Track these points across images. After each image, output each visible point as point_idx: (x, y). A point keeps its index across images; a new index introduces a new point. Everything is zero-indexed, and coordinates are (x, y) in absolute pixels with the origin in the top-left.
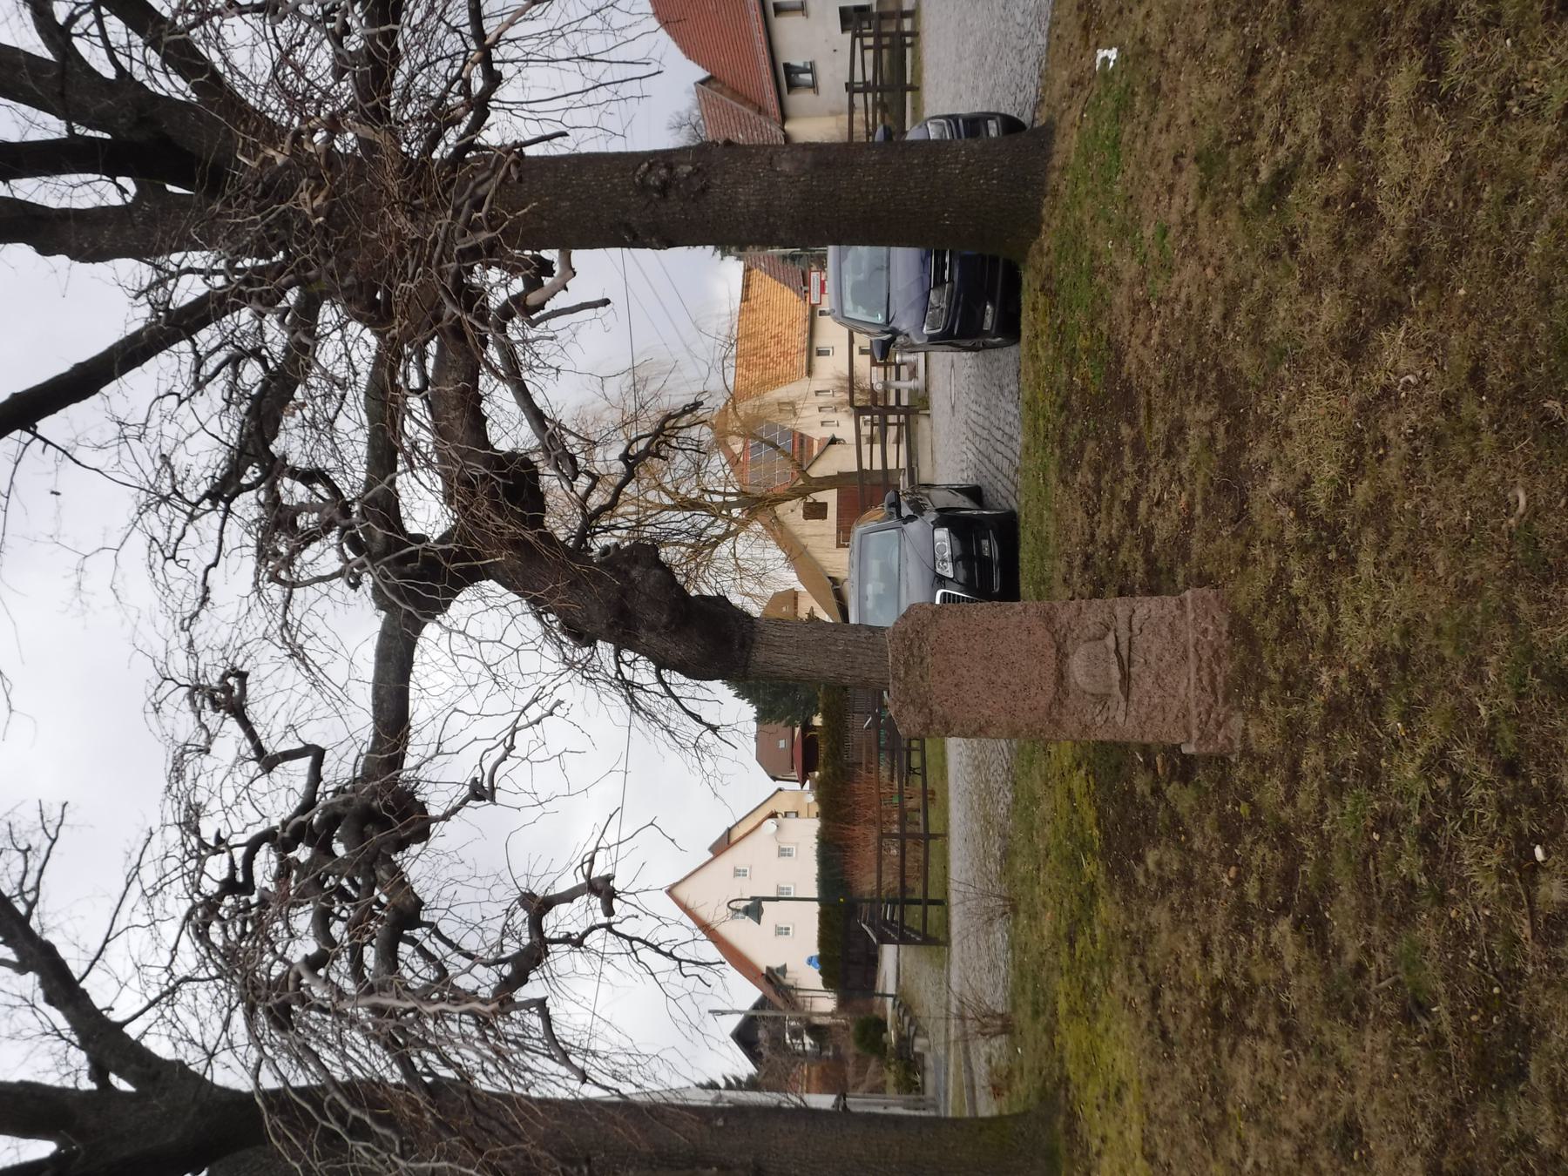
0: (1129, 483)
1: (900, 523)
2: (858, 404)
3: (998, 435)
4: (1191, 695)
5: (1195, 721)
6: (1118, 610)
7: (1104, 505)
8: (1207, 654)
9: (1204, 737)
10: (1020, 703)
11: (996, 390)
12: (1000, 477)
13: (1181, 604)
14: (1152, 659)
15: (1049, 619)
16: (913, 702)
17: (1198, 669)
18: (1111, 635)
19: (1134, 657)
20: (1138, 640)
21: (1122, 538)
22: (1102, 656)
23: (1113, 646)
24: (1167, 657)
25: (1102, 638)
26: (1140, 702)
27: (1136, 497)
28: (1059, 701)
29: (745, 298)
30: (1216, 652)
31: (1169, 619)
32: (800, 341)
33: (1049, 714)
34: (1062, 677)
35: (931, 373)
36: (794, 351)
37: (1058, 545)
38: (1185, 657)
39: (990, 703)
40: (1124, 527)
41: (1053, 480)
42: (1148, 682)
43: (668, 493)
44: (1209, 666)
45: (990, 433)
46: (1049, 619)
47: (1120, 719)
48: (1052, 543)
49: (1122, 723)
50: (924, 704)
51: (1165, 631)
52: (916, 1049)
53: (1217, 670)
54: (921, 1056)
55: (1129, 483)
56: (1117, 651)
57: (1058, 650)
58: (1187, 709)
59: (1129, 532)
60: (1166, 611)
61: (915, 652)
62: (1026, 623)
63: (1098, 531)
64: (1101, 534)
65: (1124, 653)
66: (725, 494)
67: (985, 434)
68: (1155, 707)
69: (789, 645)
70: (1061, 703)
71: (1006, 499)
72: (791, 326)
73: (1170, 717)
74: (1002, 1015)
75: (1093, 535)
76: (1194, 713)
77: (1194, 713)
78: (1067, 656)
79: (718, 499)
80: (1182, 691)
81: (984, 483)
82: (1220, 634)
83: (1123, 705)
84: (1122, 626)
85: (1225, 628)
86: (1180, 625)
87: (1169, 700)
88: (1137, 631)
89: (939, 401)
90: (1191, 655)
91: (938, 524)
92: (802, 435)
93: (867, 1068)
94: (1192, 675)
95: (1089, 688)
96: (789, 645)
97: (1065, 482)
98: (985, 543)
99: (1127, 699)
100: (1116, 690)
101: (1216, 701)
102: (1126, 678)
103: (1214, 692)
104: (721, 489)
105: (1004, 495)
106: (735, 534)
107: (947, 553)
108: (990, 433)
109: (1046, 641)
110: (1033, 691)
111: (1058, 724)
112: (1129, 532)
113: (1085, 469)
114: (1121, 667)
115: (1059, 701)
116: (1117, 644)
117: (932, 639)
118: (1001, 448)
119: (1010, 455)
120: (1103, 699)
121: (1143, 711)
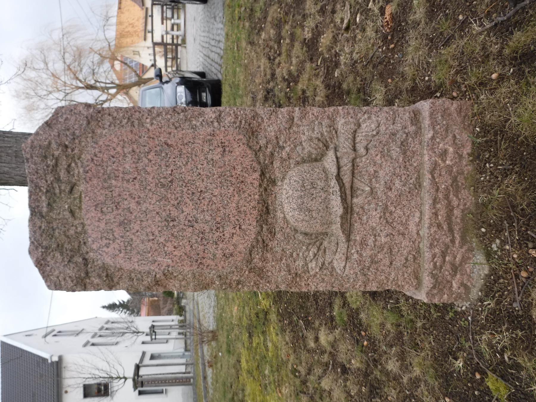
0: (310, 23)
1: (161, 85)
2: (155, 41)
3: (213, 43)
4: (424, 232)
5: (427, 266)
6: (340, 122)
7: (284, 49)
8: (445, 182)
9: (439, 284)
10: (212, 248)
11: (212, 20)
12: (213, 64)
13: (416, 118)
14: (380, 188)
15: (252, 132)
16: (60, 247)
17: (435, 201)
18: (331, 154)
19: (358, 184)
20: (362, 162)
21: (300, 71)
22: (321, 184)
23: (333, 170)
24: (398, 184)
25: (318, 159)
26: (363, 243)
27: (317, 33)
28: (262, 244)
29: (120, 8)
30: (455, 180)
31: (401, 136)
32: (141, 27)
33: (249, 261)
34: (268, 212)
35: (187, 23)
36: (139, 30)
37: (246, 87)
38: (419, 185)
39: (170, 248)
40: (303, 62)
41: (244, 44)
42: (374, 217)
43: (81, 81)
44: (447, 197)
45: (209, 44)
46: (252, 132)
47: (338, 265)
48: (242, 86)
49: (338, 268)
50: (76, 251)
51: (395, 151)
52: (182, 304)
53: (455, 202)
54: (185, 306)
55: (310, 23)
56: (339, 178)
57: (263, 174)
58: (418, 251)
59: (308, 65)
60: (398, 126)
61: (63, 174)
62: (221, 137)
63: (278, 71)
64: (281, 72)
65: (346, 179)
66: (106, 83)
67: (207, 45)
68: (382, 248)
69: (8, 155)
70: (265, 246)
71: (216, 75)
72: (138, 20)
73: (399, 262)
74: (212, 332)
75: (273, 75)
76: (427, 255)
77: (427, 255)
78: (273, 182)
79: (103, 85)
80: (412, 227)
81: (206, 70)
82: (461, 157)
83: (343, 246)
84: (345, 145)
85: (468, 149)
86: (413, 145)
87: (398, 239)
88: (362, 151)
89: (189, 39)
90: (426, 183)
91: (179, 84)
92: (143, 65)
93: (167, 301)
94: (427, 208)
95: (302, 227)
96: (8, 155)
97: (252, 43)
98: (204, 94)
99: (348, 240)
100: (336, 228)
101: (453, 241)
102: (348, 210)
103: (451, 230)
104: (104, 81)
105: (214, 74)
106: (110, 100)
107: (184, 100)
108: (209, 44)
109: (247, 162)
110: (229, 230)
111: (261, 273)
112: (308, 65)
113: (268, 26)
114: (344, 200)
115: (262, 244)
116: (339, 168)
117: (86, 157)
118: (214, 49)
119: (218, 51)
120: (317, 239)
121: (367, 253)
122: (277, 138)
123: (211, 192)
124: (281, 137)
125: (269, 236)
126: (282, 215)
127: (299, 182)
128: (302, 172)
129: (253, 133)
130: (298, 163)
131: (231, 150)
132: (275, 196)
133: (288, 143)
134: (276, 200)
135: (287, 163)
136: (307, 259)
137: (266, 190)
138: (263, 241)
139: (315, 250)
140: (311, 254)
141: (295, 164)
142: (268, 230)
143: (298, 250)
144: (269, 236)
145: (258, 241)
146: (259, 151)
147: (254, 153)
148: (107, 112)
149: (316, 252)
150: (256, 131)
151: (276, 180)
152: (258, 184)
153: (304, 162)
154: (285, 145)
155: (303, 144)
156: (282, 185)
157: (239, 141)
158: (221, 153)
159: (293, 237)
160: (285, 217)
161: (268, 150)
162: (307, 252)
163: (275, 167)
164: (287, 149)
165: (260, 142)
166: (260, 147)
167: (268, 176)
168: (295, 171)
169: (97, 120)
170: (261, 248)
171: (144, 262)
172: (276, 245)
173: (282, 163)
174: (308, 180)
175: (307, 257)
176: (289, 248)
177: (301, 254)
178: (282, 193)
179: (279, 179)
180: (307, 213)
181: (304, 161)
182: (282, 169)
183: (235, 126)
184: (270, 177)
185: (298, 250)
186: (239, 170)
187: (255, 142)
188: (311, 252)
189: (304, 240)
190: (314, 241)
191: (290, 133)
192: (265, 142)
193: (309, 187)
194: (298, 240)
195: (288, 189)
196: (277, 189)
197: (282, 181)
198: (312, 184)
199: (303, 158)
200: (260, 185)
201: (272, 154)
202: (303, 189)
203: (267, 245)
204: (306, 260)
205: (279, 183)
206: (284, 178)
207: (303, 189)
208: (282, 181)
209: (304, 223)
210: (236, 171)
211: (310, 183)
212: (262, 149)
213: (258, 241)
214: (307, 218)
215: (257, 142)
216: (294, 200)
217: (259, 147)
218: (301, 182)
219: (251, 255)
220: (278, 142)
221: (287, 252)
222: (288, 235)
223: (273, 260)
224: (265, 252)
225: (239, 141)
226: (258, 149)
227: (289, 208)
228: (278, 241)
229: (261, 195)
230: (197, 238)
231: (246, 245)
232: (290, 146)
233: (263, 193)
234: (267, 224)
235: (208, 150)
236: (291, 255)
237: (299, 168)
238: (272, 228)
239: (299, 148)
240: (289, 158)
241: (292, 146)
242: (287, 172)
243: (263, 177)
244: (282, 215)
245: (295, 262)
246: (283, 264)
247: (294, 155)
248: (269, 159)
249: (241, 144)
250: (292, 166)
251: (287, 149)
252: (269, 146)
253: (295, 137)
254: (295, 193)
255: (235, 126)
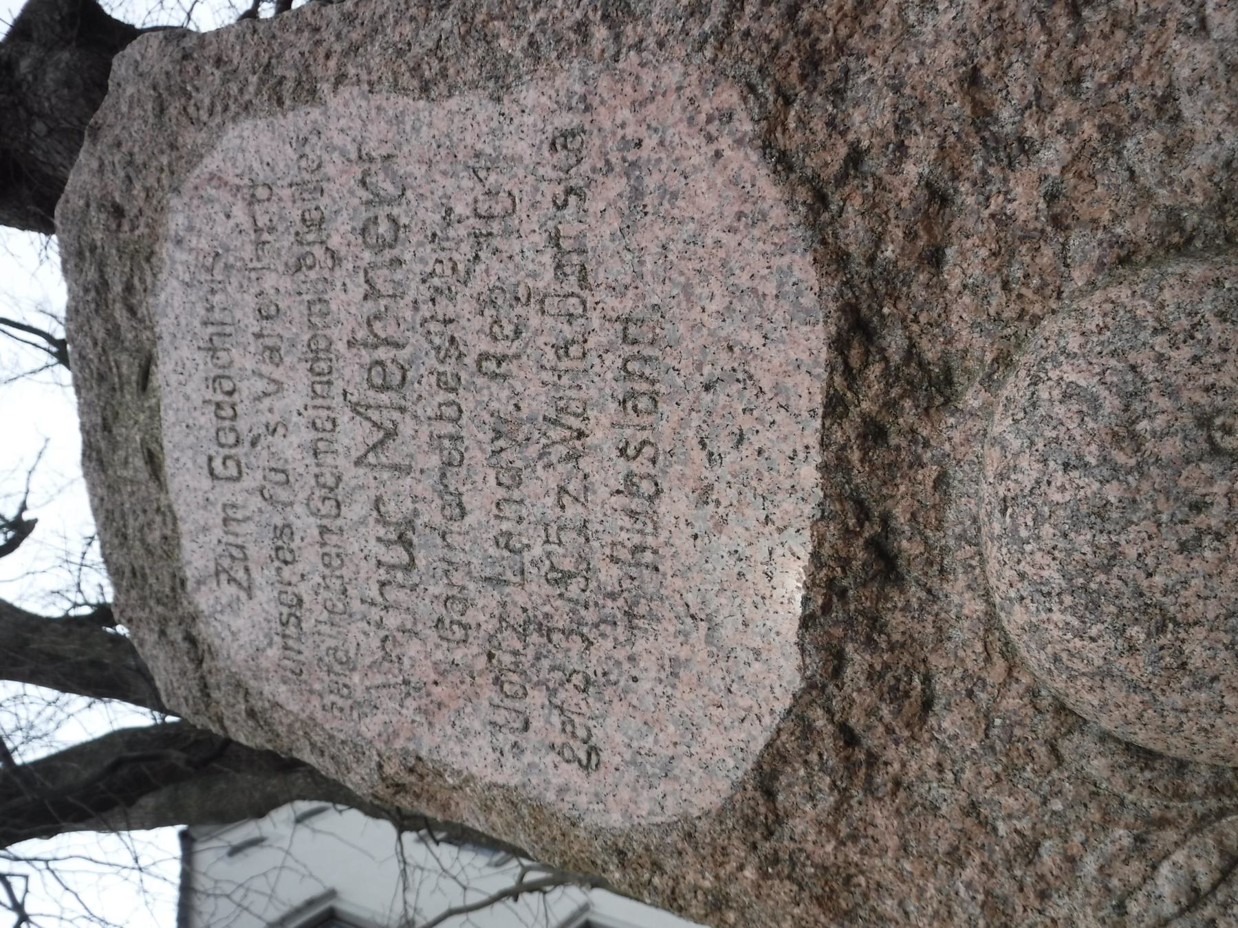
78: (937, 386)
122: (972, 80)
123: (576, 423)
124: (1002, 72)
125: (885, 711)
126: (976, 607)
127: (1095, 404)
128: (1138, 323)
129: (813, 63)
130: (1125, 258)
131: (676, 182)
132: (941, 481)
133: (1066, 109)
134: (946, 500)
135: (1047, 254)
136: (1133, 908)
137: (874, 433)
138: (849, 737)
139: (1200, 867)
140: (1166, 882)
141: (1101, 266)
142: (873, 676)
143: (1078, 836)
144: (885, 711)
145: (807, 730)
146: (842, 179)
147: (803, 194)
148: (211, 51)
149: (1204, 882)
150: (841, 47)
151: (958, 377)
152: (819, 399)
153: (1182, 249)
154: (1032, 130)
155: (1189, 107)
156: (987, 411)
157: (713, 128)
158: (623, 204)
159: (1042, 751)
160: (991, 621)
161: (911, 170)
162: (1136, 865)
163: (955, 285)
164: (1046, 155)
165: (857, 117)
166: (856, 157)
167: (894, 342)
168: (1081, 315)
169: (184, 90)
170: (831, 772)
171: (340, 702)
172: (932, 774)
173: (1003, 253)
174: (1171, 392)
175: (1130, 893)
176: (1011, 811)
177: (1090, 865)
178: (980, 462)
179: (970, 364)
180: (1136, 632)
181: (1177, 240)
182: (997, 299)
183: (695, 32)
184: (911, 353)
185: (1078, 836)
186: (712, 307)
187: (818, 125)
188: (1165, 869)
189: (1119, 785)
190: (1199, 807)
191: (1082, 38)
192: (884, 119)
193: (1171, 448)
194: (1083, 779)
195: (1015, 444)
196: (951, 431)
197: (989, 382)
198: (1204, 422)
199: (1174, 218)
200: (834, 407)
201: (938, 197)
202: (1120, 458)
203: (873, 759)
204: (1121, 908)
205: (972, 398)
206: (1004, 361)
207: (1120, 458)
208: (989, 382)
209: (1114, 691)
210: (696, 313)
211: (1187, 419)
212: (869, 164)
213: (807, 730)
214: (1138, 667)
215: (831, 123)
216: (1047, 530)
217: (843, 151)
218: (1111, 403)
219: (770, 795)
220: (982, 115)
221: (1002, 828)
222: (1008, 728)
223: (905, 847)
224: (857, 794)
225: (713, 128)
226: (836, 167)
227: (1009, 573)
228: (943, 748)
229: (834, 468)
230: (519, 646)
231: (738, 735)
232: (1068, 129)
233: (855, 456)
234: (870, 643)
235: (560, 190)
236: (1029, 850)
237: (1123, 294)
238: (908, 671)
239: (1141, 149)
240: (1056, 221)
241: (1088, 129)
242: (1036, 320)
243: (855, 354)
244: (976, 607)
245: (1043, 896)
246: (969, 885)
247: (1100, 200)
248: (910, 235)
249: (724, 143)
250: (1079, 277)
251: (1053, 156)
252: (921, 144)
253: (1122, 58)
254: (1059, 479)
255: (695, 32)
